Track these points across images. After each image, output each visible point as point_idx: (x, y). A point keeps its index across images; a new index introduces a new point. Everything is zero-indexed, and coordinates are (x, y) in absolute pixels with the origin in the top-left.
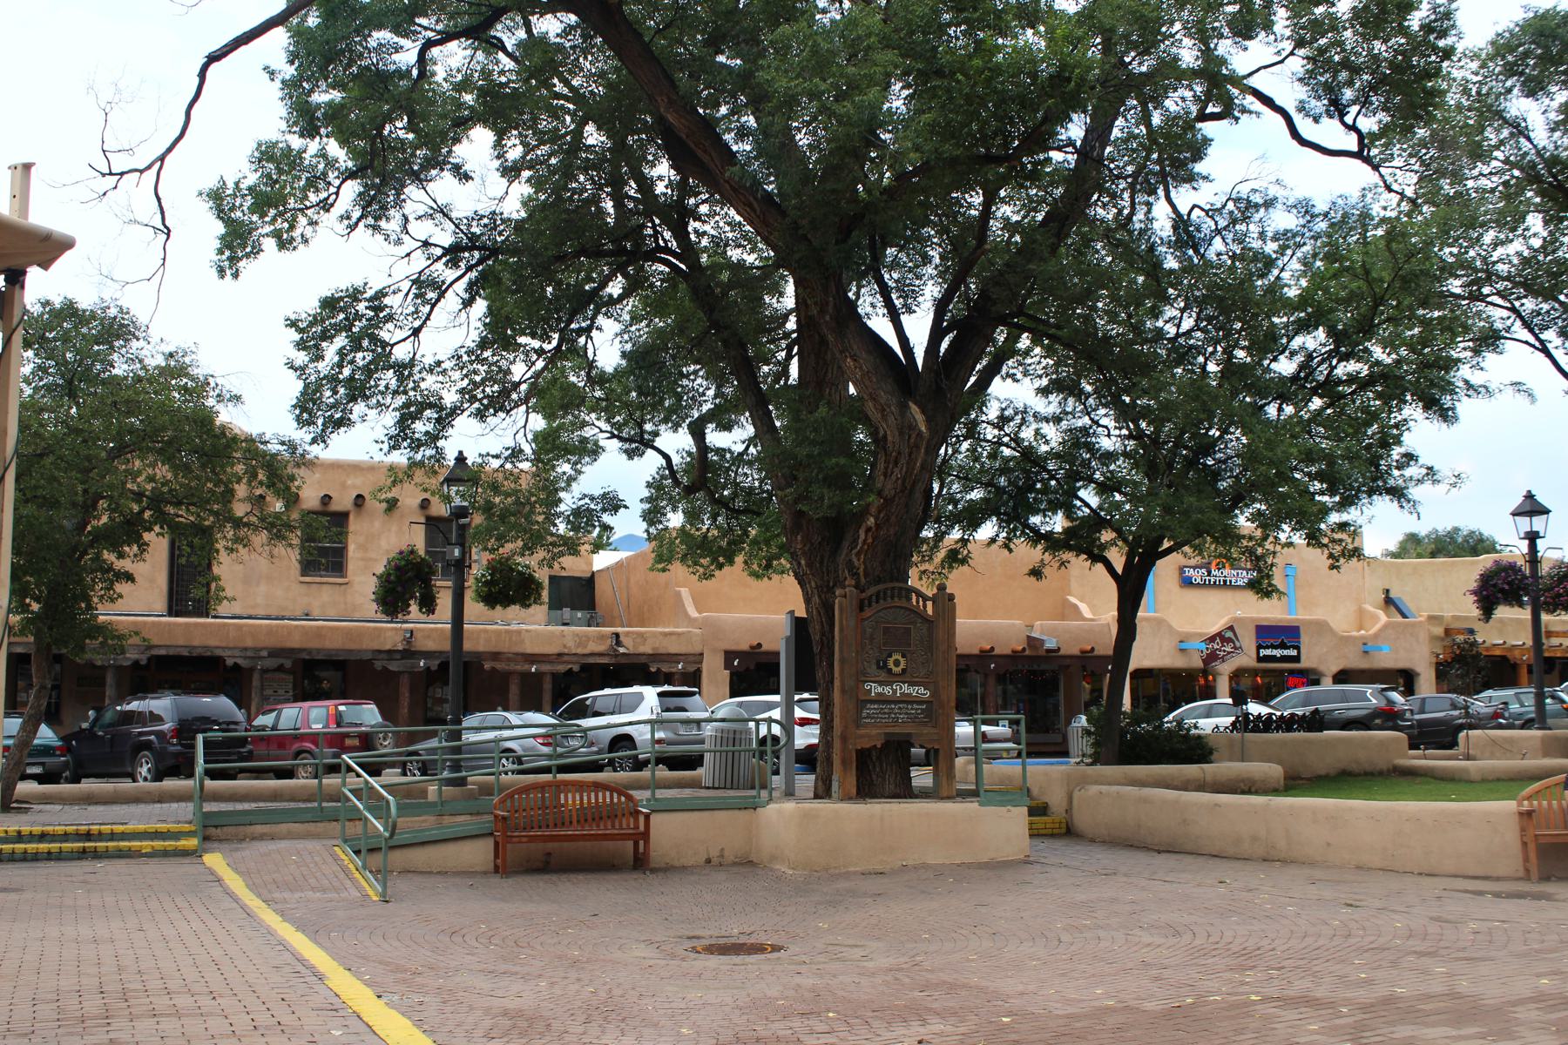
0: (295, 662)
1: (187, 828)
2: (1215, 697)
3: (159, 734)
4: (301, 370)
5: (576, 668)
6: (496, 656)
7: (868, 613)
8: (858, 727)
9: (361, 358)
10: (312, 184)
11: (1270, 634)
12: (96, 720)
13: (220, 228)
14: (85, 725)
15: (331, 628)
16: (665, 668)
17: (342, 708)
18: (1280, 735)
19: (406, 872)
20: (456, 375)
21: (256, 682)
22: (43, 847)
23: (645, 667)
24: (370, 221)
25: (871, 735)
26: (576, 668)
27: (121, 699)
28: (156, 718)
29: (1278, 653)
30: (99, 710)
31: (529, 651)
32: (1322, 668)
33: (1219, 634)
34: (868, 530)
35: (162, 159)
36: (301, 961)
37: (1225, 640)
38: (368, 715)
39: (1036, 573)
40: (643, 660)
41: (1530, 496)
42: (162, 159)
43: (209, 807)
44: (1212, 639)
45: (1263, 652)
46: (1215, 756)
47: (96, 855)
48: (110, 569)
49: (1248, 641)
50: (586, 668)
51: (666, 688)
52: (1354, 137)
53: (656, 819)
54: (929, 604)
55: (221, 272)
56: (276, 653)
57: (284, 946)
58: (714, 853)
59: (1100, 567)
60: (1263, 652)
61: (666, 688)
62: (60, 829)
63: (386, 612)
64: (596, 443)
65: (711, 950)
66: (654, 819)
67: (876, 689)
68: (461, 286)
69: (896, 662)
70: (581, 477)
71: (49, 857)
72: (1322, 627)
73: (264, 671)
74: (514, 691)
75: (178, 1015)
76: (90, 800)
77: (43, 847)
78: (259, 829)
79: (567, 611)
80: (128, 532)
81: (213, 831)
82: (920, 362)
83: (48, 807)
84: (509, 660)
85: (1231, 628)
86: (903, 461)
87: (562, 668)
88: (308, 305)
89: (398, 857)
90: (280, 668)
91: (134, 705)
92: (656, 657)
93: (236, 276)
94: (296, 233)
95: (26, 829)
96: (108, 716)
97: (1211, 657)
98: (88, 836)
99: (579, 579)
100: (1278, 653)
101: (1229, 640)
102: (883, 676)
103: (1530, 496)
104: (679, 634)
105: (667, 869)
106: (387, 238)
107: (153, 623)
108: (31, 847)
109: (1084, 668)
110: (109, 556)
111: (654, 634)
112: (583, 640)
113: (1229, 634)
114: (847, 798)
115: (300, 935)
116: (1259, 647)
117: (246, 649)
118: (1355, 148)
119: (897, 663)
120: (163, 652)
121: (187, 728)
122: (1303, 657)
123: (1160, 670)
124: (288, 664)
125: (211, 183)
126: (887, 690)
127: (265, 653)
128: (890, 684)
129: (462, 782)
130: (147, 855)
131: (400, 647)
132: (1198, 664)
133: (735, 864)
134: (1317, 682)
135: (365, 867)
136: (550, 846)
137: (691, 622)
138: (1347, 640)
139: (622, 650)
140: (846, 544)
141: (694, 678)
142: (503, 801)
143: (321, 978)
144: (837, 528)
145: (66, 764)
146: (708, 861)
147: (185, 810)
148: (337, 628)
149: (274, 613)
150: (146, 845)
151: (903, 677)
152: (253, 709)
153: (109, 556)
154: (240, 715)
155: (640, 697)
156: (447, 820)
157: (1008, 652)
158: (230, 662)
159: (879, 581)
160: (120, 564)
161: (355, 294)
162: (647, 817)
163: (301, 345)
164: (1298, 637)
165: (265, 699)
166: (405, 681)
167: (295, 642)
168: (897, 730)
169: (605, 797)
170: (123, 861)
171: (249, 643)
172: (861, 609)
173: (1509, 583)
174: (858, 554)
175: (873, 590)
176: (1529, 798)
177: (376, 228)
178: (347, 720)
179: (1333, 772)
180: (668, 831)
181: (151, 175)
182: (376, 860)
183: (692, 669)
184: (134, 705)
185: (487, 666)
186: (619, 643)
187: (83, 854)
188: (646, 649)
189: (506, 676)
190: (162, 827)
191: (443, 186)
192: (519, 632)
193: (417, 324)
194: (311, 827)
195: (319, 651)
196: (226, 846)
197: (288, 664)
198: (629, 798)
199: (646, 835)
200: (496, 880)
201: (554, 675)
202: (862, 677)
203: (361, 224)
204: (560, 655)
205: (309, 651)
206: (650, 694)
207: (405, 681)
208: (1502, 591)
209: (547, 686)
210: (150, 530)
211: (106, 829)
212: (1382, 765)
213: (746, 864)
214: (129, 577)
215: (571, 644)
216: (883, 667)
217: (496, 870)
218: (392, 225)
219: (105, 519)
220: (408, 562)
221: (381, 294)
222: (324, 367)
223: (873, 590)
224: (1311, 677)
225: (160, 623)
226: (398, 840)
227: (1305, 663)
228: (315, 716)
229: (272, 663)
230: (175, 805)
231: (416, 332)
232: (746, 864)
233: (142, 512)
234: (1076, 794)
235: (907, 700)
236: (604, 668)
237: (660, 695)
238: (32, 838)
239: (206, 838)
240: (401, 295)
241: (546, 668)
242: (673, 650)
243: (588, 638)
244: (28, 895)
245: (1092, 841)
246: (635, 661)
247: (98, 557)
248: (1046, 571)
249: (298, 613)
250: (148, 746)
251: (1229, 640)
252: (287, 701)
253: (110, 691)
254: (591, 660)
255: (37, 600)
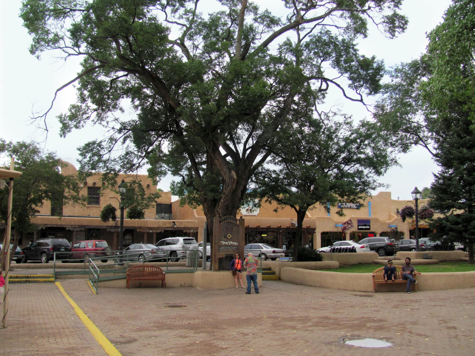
0: (85, 229)
1: (51, 275)
2: (345, 240)
3: (48, 249)
4: (80, 162)
5: (163, 231)
6: (140, 228)
7: (222, 223)
8: (219, 252)
9: (96, 158)
10: (85, 113)
11: (362, 222)
12: (32, 244)
13: (61, 125)
14: (28, 246)
15: (95, 220)
16: (188, 232)
17: (97, 242)
18: (344, 253)
19: (105, 287)
20: (120, 162)
21: (75, 233)
22: (17, 280)
23: (182, 231)
24: (99, 121)
25: (222, 254)
26: (163, 231)
27: (38, 239)
28: (47, 244)
29: (364, 227)
30: (32, 241)
31: (150, 226)
32: (377, 231)
33: (347, 222)
34: (222, 203)
35: (46, 114)
36: (71, 306)
37: (348, 224)
38: (104, 244)
39: (276, 211)
40: (182, 229)
41: (416, 188)
42: (46, 114)
43: (57, 270)
44: (345, 223)
45: (360, 227)
46: (323, 259)
47: (30, 282)
48: (34, 209)
49: (355, 224)
50: (165, 231)
51: (186, 238)
52: (360, 96)
53: (166, 275)
54: (238, 221)
55: (61, 136)
56: (80, 226)
57: (68, 303)
58: (183, 284)
59: (293, 209)
60: (360, 227)
61: (186, 238)
62: (21, 275)
63: (103, 221)
64: (165, 171)
65: (169, 307)
66: (166, 275)
67: (224, 243)
68: (121, 140)
69: (229, 236)
70: (161, 181)
71: (18, 282)
72: (376, 220)
73: (77, 231)
74: (145, 237)
75: (42, 314)
76: (29, 268)
77: (17, 280)
78: (70, 276)
79: (163, 215)
80: (38, 200)
81: (57, 276)
82: (241, 157)
83: (18, 269)
84: (144, 229)
85: (350, 220)
86: (230, 186)
87: (159, 231)
88: (82, 144)
89: (100, 284)
90: (81, 231)
91: (41, 241)
92: (185, 228)
93: (65, 137)
94: (81, 125)
95: (13, 275)
96: (35, 244)
97: (345, 229)
98: (28, 277)
99: (167, 204)
100: (364, 227)
101: (350, 224)
102: (226, 239)
103: (416, 188)
104: (192, 222)
105: (171, 287)
106: (103, 126)
107: (47, 218)
108: (14, 280)
109: (308, 232)
110: (33, 206)
111: (185, 222)
112: (165, 223)
113: (350, 222)
114: (216, 270)
115: (73, 301)
116: (358, 226)
117: (72, 225)
118: (360, 99)
119: (229, 236)
120: (49, 226)
121: (56, 248)
122: (371, 228)
123: (330, 232)
124: (83, 229)
125: (58, 114)
126: (227, 243)
127: (77, 227)
128: (228, 241)
129: (123, 265)
130: (42, 282)
131: (114, 225)
132: (341, 230)
133: (188, 286)
134: (375, 236)
135: (94, 286)
136: (141, 281)
137: (196, 218)
138: (384, 224)
139: (175, 226)
140: (217, 206)
141: (195, 235)
142: (129, 270)
143: (73, 309)
144: (215, 202)
145: (23, 257)
146: (181, 286)
147: (51, 271)
148: (96, 220)
149: (80, 215)
150: (41, 280)
151: (231, 239)
152: (74, 242)
153: (33, 206)
154: (69, 244)
155: (178, 240)
156: (117, 274)
157: (286, 227)
158: (67, 229)
159: (225, 215)
160: (37, 208)
161: (94, 143)
162: (164, 274)
163: (81, 155)
164: (370, 223)
165: (77, 239)
166: (115, 234)
167: (85, 224)
168: (229, 253)
169: (155, 269)
170: (36, 284)
171: (73, 224)
172: (220, 222)
173: (409, 212)
174: (220, 209)
175: (223, 218)
176: (376, 272)
177: (100, 123)
178: (98, 246)
179: (356, 263)
180: (170, 278)
181: (44, 118)
182: (96, 284)
183: (195, 232)
184: (41, 241)
185: (138, 231)
186: (175, 225)
187: (26, 282)
188: (182, 226)
189: (143, 233)
190: (45, 275)
191: (117, 113)
192: (147, 221)
193: (110, 149)
194: (83, 276)
195: (92, 226)
196: (61, 280)
197: (83, 229)
198: (161, 270)
199: (164, 278)
200: (126, 289)
201: (157, 233)
202: (220, 240)
203: (97, 123)
204: (158, 228)
205: (89, 226)
206: (181, 239)
207: (115, 234)
208: (407, 214)
209: (155, 236)
210: (44, 199)
211: (32, 275)
212: (371, 261)
213: (191, 286)
214: (39, 212)
215: (161, 224)
216: (225, 237)
217: (127, 287)
218: (104, 123)
219: (33, 196)
220: (109, 208)
221: (101, 142)
222: (86, 160)
223: (223, 218)
224: (374, 234)
225: (49, 218)
226: (100, 280)
227: (372, 230)
228: (88, 245)
229: (79, 229)
230: (50, 269)
231: (110, 151)
232: (191, 286)
233: (42, 194)
234: (282, 269)
235: (232, 246)
236: (172, 231)
237: (184, 240)
238: (14, 277)
239: (56, 278)
240: (106, 142)
241: (154, 231)
242: (190, 226)
243: (166, 223)
244: (13, 291)
245: (284, 281)
246: (179, 229)
247: (31, 207)
248: (278, 210)
249: (87, 215)
250: (45, 252)
251: (350, 224)
252: (83, 240)
253: (35, 236)
254: (167, 229)
255: (16, 217)
